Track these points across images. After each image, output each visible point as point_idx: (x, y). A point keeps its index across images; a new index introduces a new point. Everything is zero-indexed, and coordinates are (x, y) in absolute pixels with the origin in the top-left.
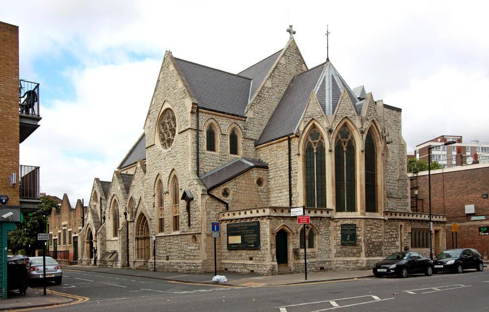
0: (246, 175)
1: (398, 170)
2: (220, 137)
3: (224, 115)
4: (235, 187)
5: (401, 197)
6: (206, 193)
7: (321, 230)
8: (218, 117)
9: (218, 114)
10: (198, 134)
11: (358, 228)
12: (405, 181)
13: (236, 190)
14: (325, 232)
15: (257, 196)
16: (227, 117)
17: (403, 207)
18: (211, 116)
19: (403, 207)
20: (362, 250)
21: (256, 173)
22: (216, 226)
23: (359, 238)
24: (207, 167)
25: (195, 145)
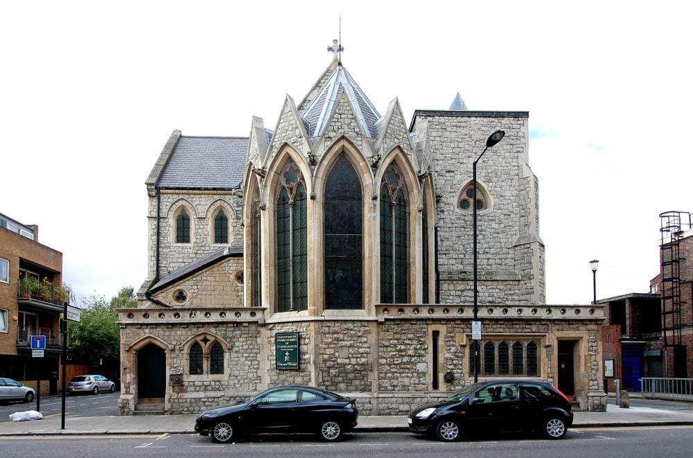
0: (215, 269)
1: (517, 228)
2: (196, 222)
3: (201, 192)
4: (195, 287)
5: (520, 277)
6: (145, 298)
7: (237, 344)
8: (192, 196)
9: (191, 191)
10: (159, 222)
11: (305, 339)
12: (528, 246)
13: (196, 291)
14: (247, 347)
15: (234, 297)
16: (207, 194)
17: (523, 298)
18: (217, 197)
19: (523, 298)
20: (310, 379)
21: (235, 265)
22: (38, 341)
23: (306, 357)
24: (174, 265)
25: (155, 238)
